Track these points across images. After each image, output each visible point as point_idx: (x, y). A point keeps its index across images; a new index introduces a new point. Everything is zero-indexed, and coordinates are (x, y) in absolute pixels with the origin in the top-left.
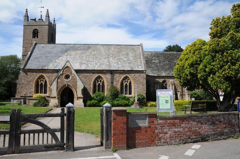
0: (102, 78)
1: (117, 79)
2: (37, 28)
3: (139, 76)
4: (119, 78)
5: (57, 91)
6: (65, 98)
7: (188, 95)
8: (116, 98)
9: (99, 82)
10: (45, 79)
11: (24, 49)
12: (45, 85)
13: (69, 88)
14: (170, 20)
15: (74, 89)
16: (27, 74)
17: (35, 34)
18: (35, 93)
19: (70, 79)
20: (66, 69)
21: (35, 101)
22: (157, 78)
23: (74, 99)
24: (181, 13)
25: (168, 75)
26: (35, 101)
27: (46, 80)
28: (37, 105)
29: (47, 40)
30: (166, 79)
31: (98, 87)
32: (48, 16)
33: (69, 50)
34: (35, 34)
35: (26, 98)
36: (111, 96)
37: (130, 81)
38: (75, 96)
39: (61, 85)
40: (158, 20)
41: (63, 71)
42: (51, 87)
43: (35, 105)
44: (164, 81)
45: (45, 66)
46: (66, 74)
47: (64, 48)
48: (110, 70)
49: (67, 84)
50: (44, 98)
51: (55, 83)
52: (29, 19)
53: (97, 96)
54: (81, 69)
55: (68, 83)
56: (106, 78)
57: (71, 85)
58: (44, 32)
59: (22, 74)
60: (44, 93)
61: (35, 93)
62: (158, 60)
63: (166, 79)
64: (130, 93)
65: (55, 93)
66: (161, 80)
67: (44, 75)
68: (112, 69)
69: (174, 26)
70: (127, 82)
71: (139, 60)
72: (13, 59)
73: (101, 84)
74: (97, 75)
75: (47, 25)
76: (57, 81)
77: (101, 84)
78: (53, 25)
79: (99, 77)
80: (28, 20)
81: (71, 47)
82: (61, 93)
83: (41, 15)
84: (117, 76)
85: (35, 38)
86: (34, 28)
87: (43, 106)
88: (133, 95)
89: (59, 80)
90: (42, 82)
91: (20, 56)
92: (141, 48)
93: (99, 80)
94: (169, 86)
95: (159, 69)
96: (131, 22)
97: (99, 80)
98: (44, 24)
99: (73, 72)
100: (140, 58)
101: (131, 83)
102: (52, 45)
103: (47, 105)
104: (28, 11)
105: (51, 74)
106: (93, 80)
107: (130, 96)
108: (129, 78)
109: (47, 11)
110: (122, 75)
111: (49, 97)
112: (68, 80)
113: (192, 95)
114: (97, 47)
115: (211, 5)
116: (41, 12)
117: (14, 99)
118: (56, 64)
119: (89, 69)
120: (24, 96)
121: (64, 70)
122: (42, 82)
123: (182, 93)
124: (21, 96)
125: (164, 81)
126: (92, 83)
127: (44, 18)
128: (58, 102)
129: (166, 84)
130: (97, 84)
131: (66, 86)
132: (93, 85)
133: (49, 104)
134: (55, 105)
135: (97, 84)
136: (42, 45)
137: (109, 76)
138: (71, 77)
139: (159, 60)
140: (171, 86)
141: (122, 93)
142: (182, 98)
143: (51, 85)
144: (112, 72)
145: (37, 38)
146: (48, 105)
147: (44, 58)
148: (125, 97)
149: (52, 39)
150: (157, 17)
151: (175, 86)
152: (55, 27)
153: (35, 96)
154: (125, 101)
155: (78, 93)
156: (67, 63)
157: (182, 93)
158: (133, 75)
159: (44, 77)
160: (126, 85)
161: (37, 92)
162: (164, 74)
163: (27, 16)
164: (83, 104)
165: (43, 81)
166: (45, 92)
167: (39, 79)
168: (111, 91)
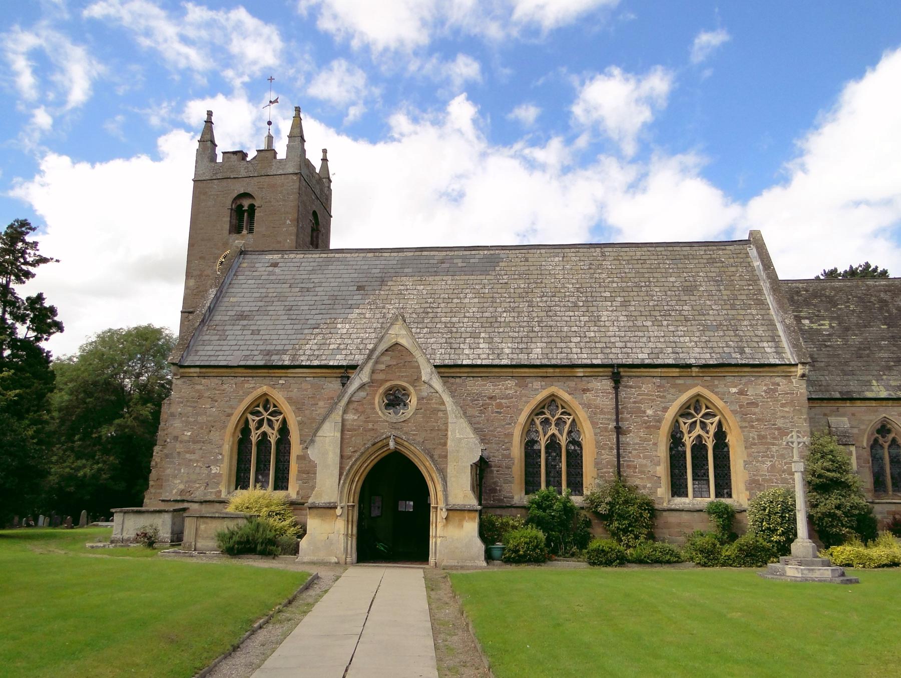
1: (649, 412)
10: (281, 413)
12: (278, 442)
15: (429, 463)
17: (242, 215)
27: (284, 422)
29: (290, 241)
33: (397, 274)
34: (242, 215)
35: (184, 510)
38: (436, 498)
39: (360, 443)
45: (284, 352)
46: (388, 385)
55: (398, 433)
58: (278, 210)
59: (180, 390)
60: (276, 488)
62: (832, 319)
67: (279, 397)
70: (704, 426)
73: (563, 440)
77: (563, 440)
93: (553, 421)
95: (846, 363)
97: (553, 421)
98: (281, 172)
99: (426, 372)
100: (761, 303)
102: (316, 256)
104: (213, 119)
106: (522, 418)
122: (265, 428)
127: (281, 149)
131: (392, 445)
136: (270, 257)
138: (413, 401)
144: (617, 373)
145: (251, 231)
147: (272, 309)
149: (314, 227)
152: (329, 187)
155: (453, 487)
164: (479, 547)
166: (281, 483)
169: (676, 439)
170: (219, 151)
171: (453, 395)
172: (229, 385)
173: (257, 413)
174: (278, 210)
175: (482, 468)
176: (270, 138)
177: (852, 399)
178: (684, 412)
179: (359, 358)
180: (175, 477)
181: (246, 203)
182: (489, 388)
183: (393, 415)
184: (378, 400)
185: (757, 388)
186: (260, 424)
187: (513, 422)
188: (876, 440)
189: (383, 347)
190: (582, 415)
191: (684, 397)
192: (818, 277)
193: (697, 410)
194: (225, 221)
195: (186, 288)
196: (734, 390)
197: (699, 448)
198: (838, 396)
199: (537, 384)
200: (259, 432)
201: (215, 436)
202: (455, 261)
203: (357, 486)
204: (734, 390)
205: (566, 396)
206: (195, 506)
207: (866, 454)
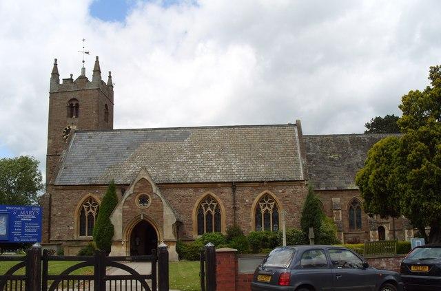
0: (214, 199)
9: (209, 209)
19: (149, 205)
32: (97, 70)
34: (73, 108)
70: (269, 206)
73: (213, 213)
77: (213, 213)
86: (71, 96)
90: (91, 210)
99: (155, 189)
102: (106, 134)
104: (58, 62)
106: (196, 205)
109: (95, 59)
122: (91, 210)
130: (205, 213)
135: (205, 213)
138: (150, 201)
144: (234, 185)
145: (77, 116)
155: (166, 234)
163: (55, 74)
169: (258, 210)
170: (61, 78)
171: (165, 197)
172: (75, 194)
173: (87, 205)
174: (89, 106)
175: (178, 225)
176: (84, 69)
177: (342, 190)
178: (261, 200)
179: (129, 181)
180: (55, 231)
181: (74, 103)
182: (182, 192)
184: (137, 201)
185: (289, 191)
186: (89, 209)
187: (192, 206)
188: (351, 207)
189: (137, 180)
190: (221, 203)
191: (261, 194)
192: (428, 88)
193: (267, 200)
194: (65, 112)
195: (48, 144)
196: (280, 191)
197: (267, 213)
198: (336, 188)
199: (202, 190)
201: (70, 214)
203: (130, 232)
204: (280, 191)
205: (214, 195)
206: (64, 243)
207: (347, 213)
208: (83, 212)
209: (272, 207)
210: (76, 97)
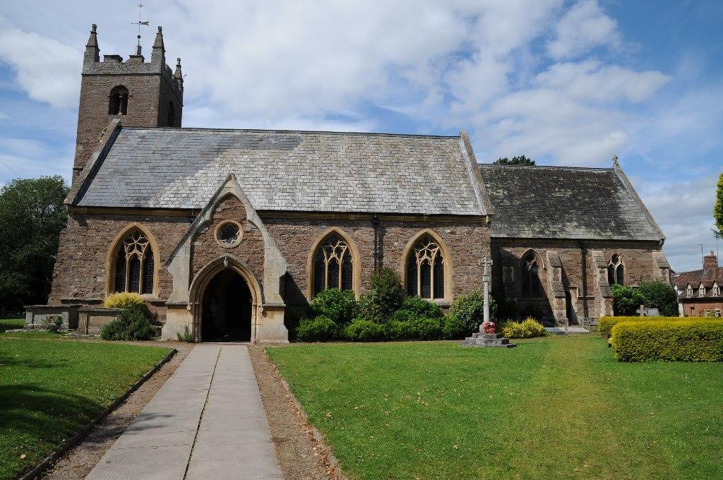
0: (342, 238)
2: (125, 82)
3: (469, 233)
4: (401, 241)
5: (190, 286)
6: (214, 308)
7: (604, 297)
8: (397, 308)
9: (333, 255)
10: (146, 241)
11: (81, 148)
13: (235, 272)
14: (486, 107)
15: (252, 277)
16: (86, 225)
17: (119, 101)
18: (110, 291)
20: (223, 205)
21: (109, 320)
22: (505, 246)
23: (253, 313)
24: (515, 90)
25: (541, 236)
26: (109, 320)
27: (149, 247)
28: (117, 335)
30: (536, 250)
31: (331, 270)
32: (160, 47)
34: (119, 101)
36: (377, 302)
37: (439, 252)
39: (204, 262)
40: (455, 107)
41: (213, 213)
42: (170, 269)
43: (109, 334)
44: (530, 256)
46: (223, 222)
47: (214, 141)
48: (373, 214)
49: (229, 259)
50: (142, 308)
51: (183, 256)
52: (101, 54)
53: (329, 304)
54: (272, 209)
55: (231, 256)
56: (358, 242)
57: (243, 261)
58: (146, 94)
60: (144, 292)
61: (110, 291)
62: (504, 189)
63: (536, 250)
64: (439, 293)
65: (181, 291)
66: (520, 253)
67: (145, 228)
68: (378, 211)
69: (497, 122)
70: (429, 254)
71: (462, 182)
72: (51, 188)
73: (340, 261)
74: (328, 230)
75: (157, 74)
76: (192, 247)
77: (340, 261)
78: (176, 79)
79: (334, 237)
80: (97, 59)
81: (235, 140)
82: (204, 288)
83: (140, 48)
84: (392, 231)
85: (116, 113)
86: (117, 82)
87: (139, 339)
88: (448, 298)
89: (196, 243)
90: (135, 251)
91: (68, 182)
92: (462, 144)
94: (545, 269)
95: (511, 217)
96: (385, 107)
100: (465, 177)
101: (441, 258)
102: (173, 132)
103: (154, 336)
105: (168, 226)
107: (438, 301)
108: (433, 240)
109: (157, 31)
110: (410, 230)
111: (161, 304)
112: (227, 245)
113: (620, 297)
114: (322, 138)
115: (590, 72)
116: (139, 37)
117: (35, 312)
118: (184, 192)
119: (299, 209)
120: (72, 301)
121: (217, 206)
122: (135, 251)
123: (585, 293)
124: (63, 301)
125: (530, 256)
126: (310, 256)
127: (148, 55)
128: (195, 324)
129: (535, 263)
130: (327, 262)
131: (225, 263)
132: (313, 261)
133: (160, 330)
134: (182, 335)
135: (327, 262)
137: (367, 233)
139: (508, 189)
140: (550, 270)
141: (411, 291)
142: (586, 308)
143: (170, 260)
144: (379, 221)
146: (157, 333)
147: (141, 170)
148: (428, 307)
149: (170, 114)
150: (454, 99)
151: (563, 272)
152: (182, 85)
153: (111, 300)
154: (430, 320)
156: (227, 181)
157: (585, 293)
158: (449, 231)
159: (143, 234)
160: (425, 266)
161: (117, 286)
162: (527, 233)
163: (93, 47)
164: (284, 331)
165: (139, 248)
166: (147, 288)
167: (124, 242)
168: (376, 284)
176: (140, 48)
183: (226, 243)
196: (449, 231)
200: (131, 254)
202: (270, 140)
208: (122, 253)
209: (434, 255)
210: (124, 84)
